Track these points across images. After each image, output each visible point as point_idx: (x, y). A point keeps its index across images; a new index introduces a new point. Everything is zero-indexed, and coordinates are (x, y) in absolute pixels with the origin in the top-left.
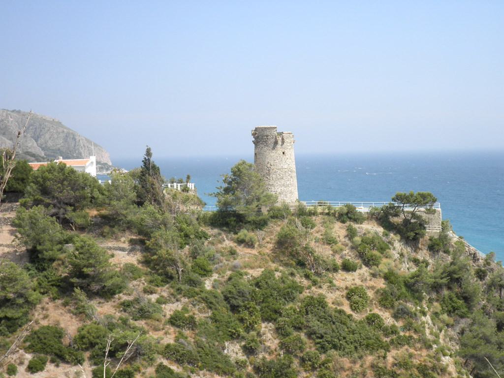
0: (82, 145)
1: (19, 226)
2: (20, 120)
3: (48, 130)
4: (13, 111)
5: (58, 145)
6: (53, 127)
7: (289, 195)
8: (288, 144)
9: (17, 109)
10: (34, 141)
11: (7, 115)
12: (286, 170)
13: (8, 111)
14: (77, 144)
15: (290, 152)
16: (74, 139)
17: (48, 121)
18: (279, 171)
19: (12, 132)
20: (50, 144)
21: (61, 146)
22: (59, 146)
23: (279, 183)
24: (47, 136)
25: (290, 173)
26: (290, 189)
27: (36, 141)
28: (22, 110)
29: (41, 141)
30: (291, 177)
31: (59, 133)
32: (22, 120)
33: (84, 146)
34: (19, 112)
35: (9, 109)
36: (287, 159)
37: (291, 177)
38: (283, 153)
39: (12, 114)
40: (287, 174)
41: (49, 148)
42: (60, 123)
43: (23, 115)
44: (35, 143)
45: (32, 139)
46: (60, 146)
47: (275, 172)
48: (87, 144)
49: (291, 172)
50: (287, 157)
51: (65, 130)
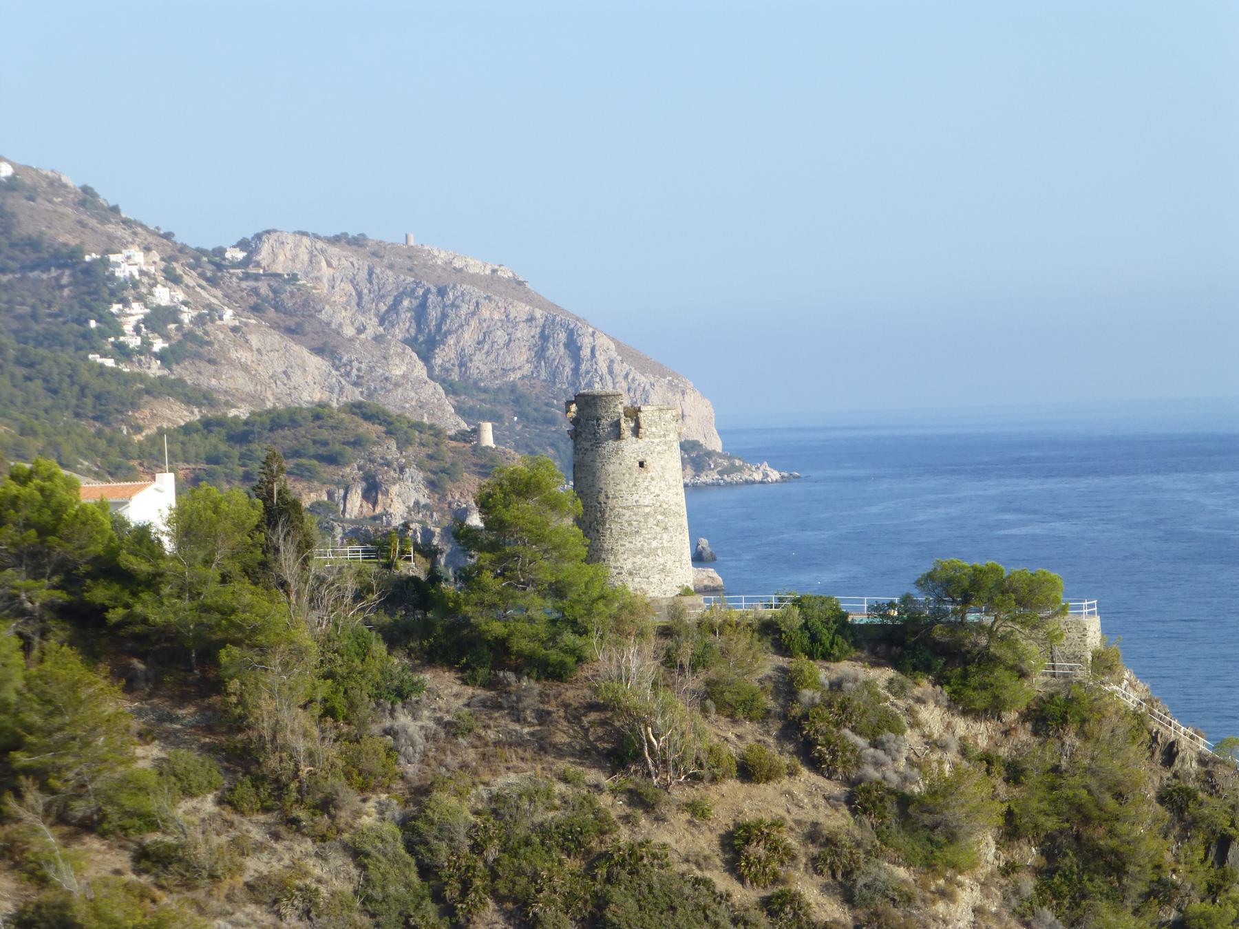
0: (605, 370)
1: (575, 737)
2: (363, 275)
3: (473, 314)
4: (335, 240)
5: (514, 370)
6: (489, 298)
7: (655, 578)
8: (656, 441)
9: (353, 233)
10: (415, 356)
11: (312, 256)
12: (647, 510)
13: (317, 237)
14: (583, 367)
15: (662, 463)
16: (573, 347)
17: (475, 279)
18: (628, 513)
19: (328, 324)
20: (479, 365)
21: (523, 377)
22: (513, 377)
23: (628, 545)
24: (469, 337)
25: (659, 517)
26: (661, 560)
27: (426, 358)
28: (373, 235)
29: (442, 357)
30: (665, 529)
31: (515, 325)
32: (371, 273)
33: (611, 372)
34: (357, 242)
35: (322, 234)
36: (652, 479)
37: (665, 529)
38: (641, 464)
39: (334, 250)
40: (651, 521)
41: (476, 383)
42: (520, 283)
43: (375, 254)
44: (420, 364)
45: (409, 350)
46: (519, 374)
47: (619, 516)
48: (626, 367)
49: (664, 514)
50: (653, 474)
51: (538, 313)
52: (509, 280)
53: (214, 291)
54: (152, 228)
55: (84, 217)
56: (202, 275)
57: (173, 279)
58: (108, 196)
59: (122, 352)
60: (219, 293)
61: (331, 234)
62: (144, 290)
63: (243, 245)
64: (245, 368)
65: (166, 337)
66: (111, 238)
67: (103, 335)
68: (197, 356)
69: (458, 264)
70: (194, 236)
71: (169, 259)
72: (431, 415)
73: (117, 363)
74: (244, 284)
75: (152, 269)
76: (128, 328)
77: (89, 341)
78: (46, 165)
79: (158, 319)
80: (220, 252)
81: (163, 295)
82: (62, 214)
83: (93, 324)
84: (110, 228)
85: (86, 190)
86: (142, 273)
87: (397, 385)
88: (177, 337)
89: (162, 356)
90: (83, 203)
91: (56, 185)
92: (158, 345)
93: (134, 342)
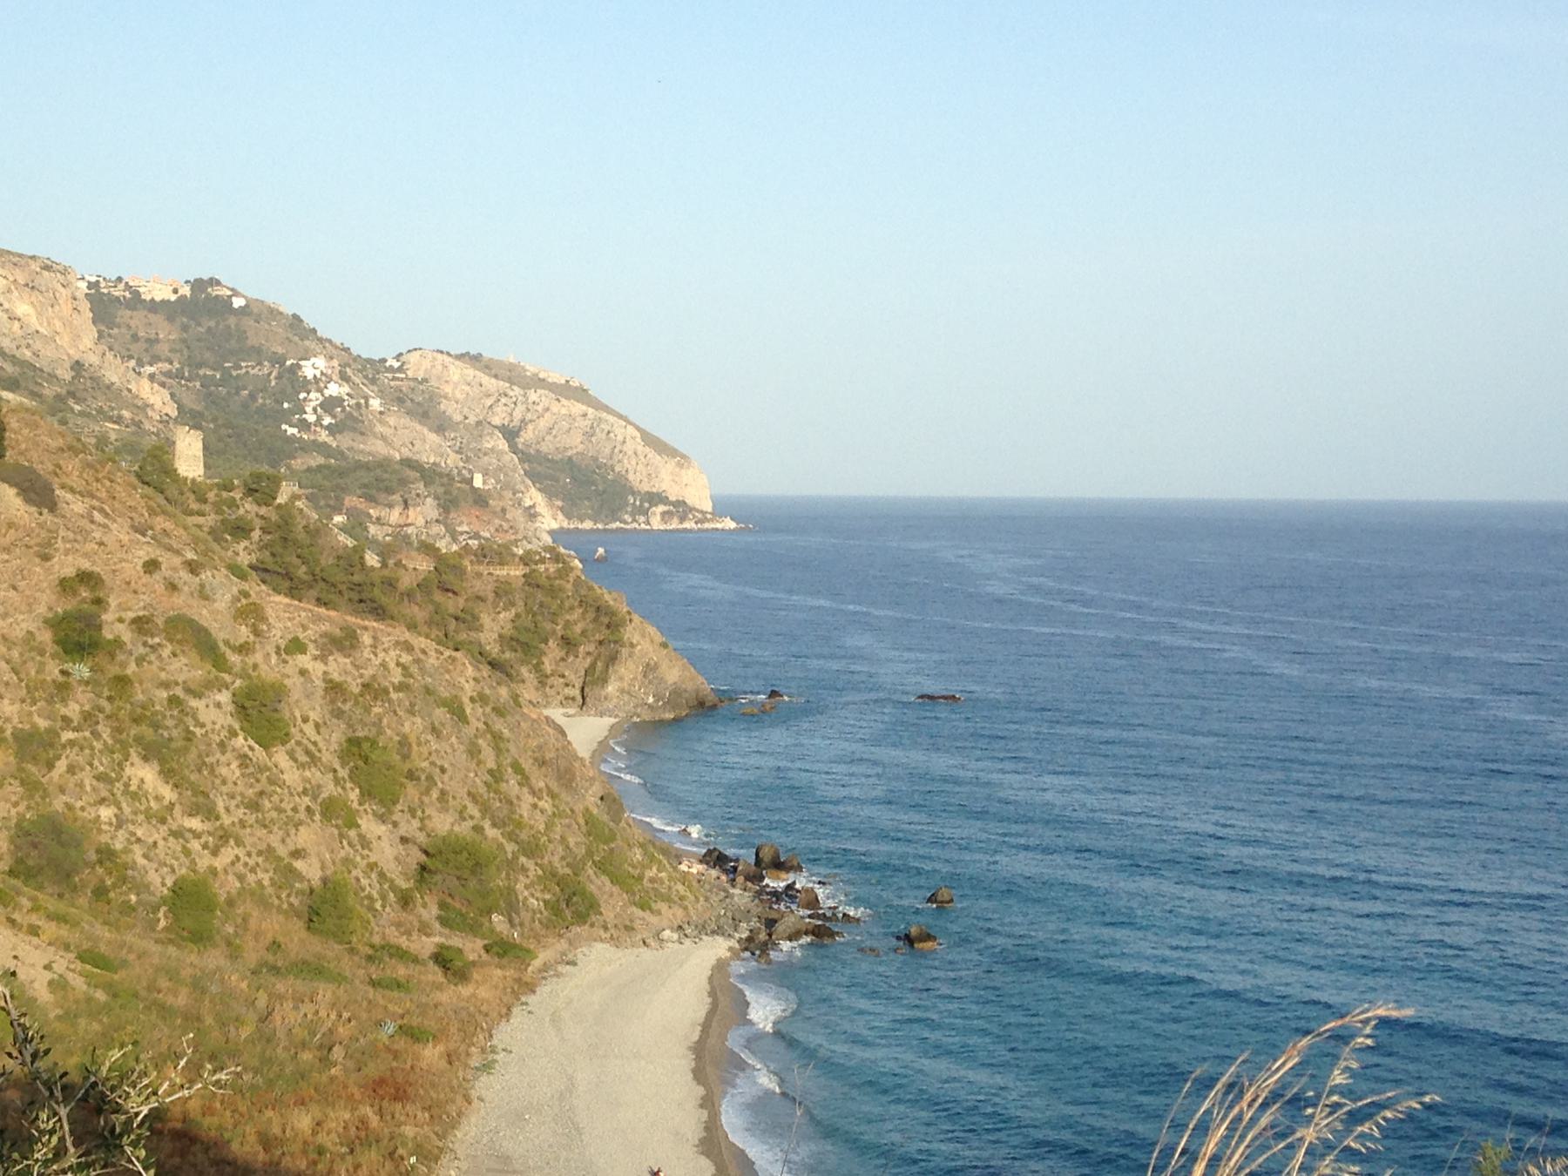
4: (460, 357)
22: (569, 453)
46: (575, 451)
52: (576, 388)
53: (371, 387)
54: (338, 344)
55: (290, 335)
56: (366, 377)
57: (345, 378)
58: (309, 321)
59: (304, 425)
60: (376, 389)
61: (459, 352)
62: (322, 385)
63: (398, 357)
64: (383, 438)
65: (334, 417)
66: (307, 350)
67: (292, 412)
68: (354, 430)
69: (541, 376)
70: (364, 349)
71: (343, 365)
72: (506, 475)
73: (1428, 1119)
74: (392, 383)
75: (330, 372)
76: (309, 409)
77: (285, 417)
78: (271, 298)
79: (329, 405)
80: (384, 360)
81: (333, 390)
82: (1461, 658)
83: (286, 405)
84: (307, 343)
85: (295, 317)
86: (322, 373)
87: (485, 454)
88: (341, 416)
89: (328, 428)
90: (291, 326)
91: (274, 313)
92: (327, 420)
93: (311, 418)
